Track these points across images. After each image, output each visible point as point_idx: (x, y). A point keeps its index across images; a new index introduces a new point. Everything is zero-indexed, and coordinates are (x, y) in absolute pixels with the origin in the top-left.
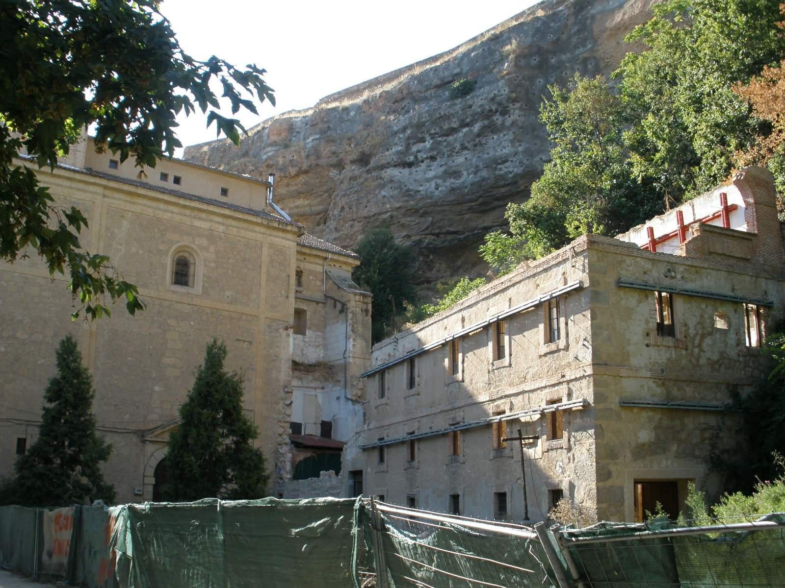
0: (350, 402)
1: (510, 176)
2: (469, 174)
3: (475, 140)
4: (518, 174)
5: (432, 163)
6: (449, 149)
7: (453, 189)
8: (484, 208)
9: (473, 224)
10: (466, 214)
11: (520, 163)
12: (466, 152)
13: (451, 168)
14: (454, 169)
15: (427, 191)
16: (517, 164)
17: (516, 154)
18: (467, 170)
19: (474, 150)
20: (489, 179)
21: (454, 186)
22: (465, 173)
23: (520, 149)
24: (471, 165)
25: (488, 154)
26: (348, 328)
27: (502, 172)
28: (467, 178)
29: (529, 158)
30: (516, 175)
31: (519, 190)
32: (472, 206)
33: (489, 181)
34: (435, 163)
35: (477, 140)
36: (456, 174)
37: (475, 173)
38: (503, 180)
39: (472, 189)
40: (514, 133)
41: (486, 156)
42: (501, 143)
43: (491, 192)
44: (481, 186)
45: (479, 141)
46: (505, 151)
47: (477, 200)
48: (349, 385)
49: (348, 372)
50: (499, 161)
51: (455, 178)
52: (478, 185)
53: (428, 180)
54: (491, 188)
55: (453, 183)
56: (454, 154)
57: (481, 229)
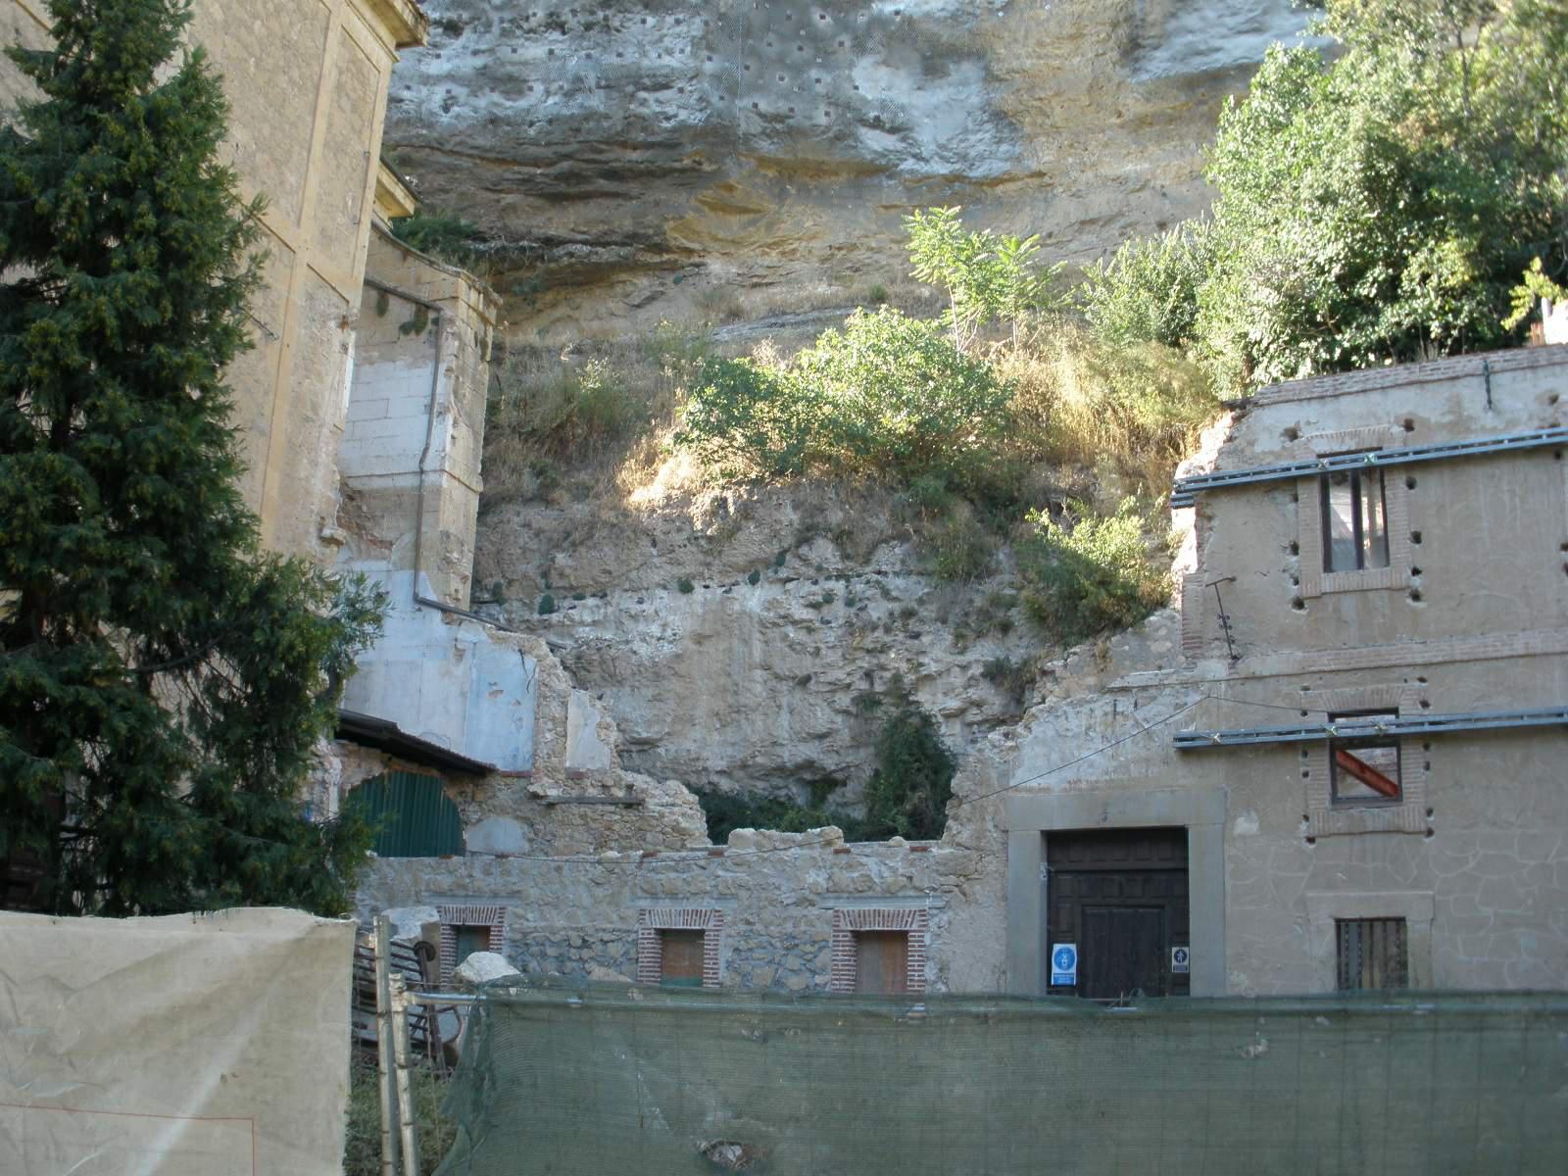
0: (437, 615)
1: (666, 125)
2: (548, 93)
3: (593, 13)
4: (690, 127)
5: (446, 40)
6: (507, 15)
7: (494, 121)
8: (562, 187)
9: (517, 223)
10: (509, 192)
11: (701, 99)
12: (556, 35)
13: (503, 64)
14: (509, 68)
15: (420, 105)
16: (692, 101)
17: (696, 75)
18: (546, 81)
19: (582, 37)
20: (607, 117)
21: (499, 112)
22: (539, 88)
23: (709, 67)
24: (562, 72)
25: (620, 55)
26: (442, 380)
27: (645, 111)
28: (541, 102)
29: (727, 97)
30: (683, 127)
31: (677, 165)
32: (535, 175)
33: (605, 124)
34: (457, 44)
35: (601, 14)
36: (513, 84)
37: (569, 95)
38: (644, 129)
39: (548, 133)
40: (706, 23)
41: (615, 60)
42: (661, 39)
43: (601, 152)
44: (578, 130)
45: (606, 18)
46: (667, 60)
47: (552, 164)
48: (429, 557)
49: (427, 518)
50: (647, 81)
51: (507, 94)
52: (574, 126)
53: (427, 80)
54: (607, 143)
55: (496, 104)
56: (518, 32)
57: (537, 240)
